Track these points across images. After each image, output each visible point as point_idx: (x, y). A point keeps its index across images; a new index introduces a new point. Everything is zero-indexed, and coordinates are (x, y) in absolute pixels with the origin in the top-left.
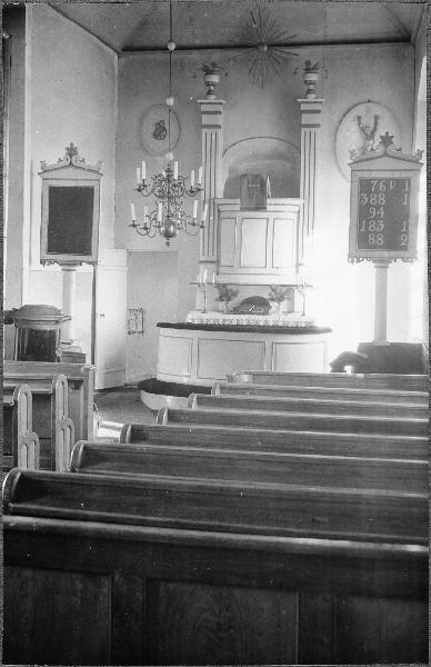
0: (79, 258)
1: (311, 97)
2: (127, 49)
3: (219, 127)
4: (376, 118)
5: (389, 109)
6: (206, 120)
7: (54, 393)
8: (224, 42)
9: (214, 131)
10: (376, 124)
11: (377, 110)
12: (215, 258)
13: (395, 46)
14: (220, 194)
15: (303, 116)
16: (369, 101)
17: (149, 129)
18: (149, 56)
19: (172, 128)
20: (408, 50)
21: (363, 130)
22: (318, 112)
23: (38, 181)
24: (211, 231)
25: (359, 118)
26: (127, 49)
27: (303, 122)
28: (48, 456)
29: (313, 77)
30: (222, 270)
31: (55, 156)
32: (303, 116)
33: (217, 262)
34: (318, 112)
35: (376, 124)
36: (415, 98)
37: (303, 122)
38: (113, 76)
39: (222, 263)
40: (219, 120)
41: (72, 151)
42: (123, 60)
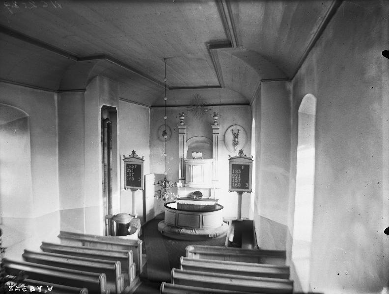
0: (137, 188)
1: (216, 124)
2: (153, 106)
3: (184, 134)
4: (238, 130)
5: (244, 130)
6: (180, 131)
7: (128, 258)
8: (188, 104)
9: (183, 135)
10: (238, 133)
11: (238, 128)
12: (183, 178)
13: (244, 106)
14: (185, 157)
15: (213, 130)
16: (236, 125)
17: (161, 133)
18: (160, 109)
19: (168, 132)
20: (249, 107)
21: (234, 134)
22: (218, 129)
23: (123, 162)
24: (181, 140)
25: (232, 130)
26: (153, 106)
27: (213, 132)
28: (127, 282)
29: (216, 118)
30: (186, 182)
31: (129, 153)
32: (213, 130)
33: (185, 179)
34: (218, 129)
35: (238, 133)
36: (251, 128)
37: (213, 132)
38: (148, 114)
39: (186, 180)
40: (185, 131)
41: (134, 152)
42: (152, 110)
